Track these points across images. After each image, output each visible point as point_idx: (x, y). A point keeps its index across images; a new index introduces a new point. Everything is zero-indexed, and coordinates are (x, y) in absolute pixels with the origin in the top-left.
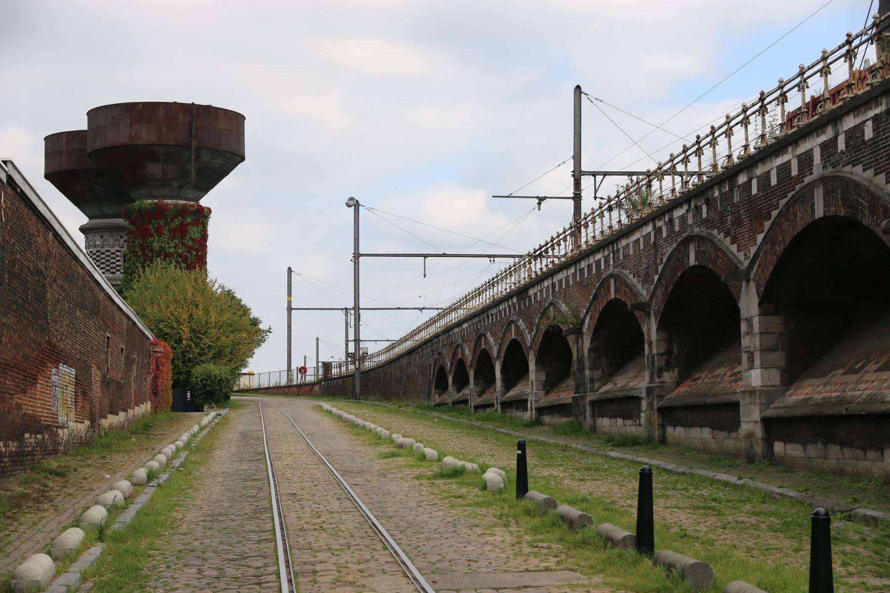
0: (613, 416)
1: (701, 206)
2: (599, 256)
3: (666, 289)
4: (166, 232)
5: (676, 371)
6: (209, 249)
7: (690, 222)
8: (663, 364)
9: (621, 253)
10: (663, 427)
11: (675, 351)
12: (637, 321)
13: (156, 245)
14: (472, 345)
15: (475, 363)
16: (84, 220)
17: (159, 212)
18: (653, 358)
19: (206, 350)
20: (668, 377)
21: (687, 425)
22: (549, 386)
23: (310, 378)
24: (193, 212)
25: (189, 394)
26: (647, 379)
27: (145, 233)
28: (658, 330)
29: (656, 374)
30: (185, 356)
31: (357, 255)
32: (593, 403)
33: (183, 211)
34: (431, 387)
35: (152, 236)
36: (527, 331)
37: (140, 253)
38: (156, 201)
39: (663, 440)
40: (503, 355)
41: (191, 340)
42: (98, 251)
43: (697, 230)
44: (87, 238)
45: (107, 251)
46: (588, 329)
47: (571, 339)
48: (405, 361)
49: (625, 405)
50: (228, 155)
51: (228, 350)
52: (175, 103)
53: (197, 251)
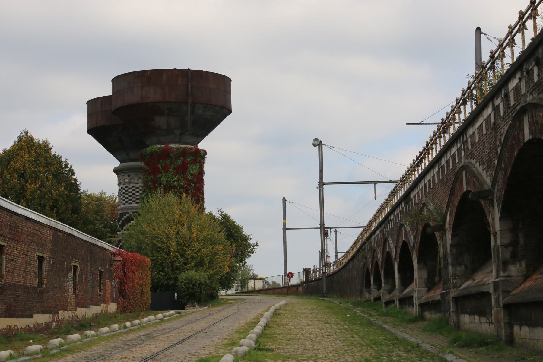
0: (471, 313)
1: (532, 69)
2: (454, 150)
3: (506, 173)
4: (171, 170)
5: (523, 263)
6: (205, 182)
7: (523, 91)
8: (508, 256)
9: (469, 143)
10: (510, 325)
11: (522, 241)
12: (484, 212)
13: (163, 180)
14: (381, 248)
15: (384, 265)
16: (117, 163)
17: (165, 154)
18: (498, 249)
19: (190, 260)
20: (514, 270)
21: (532, 324)
22: (430, 284)
23: (294, 281)
24: (192, 153)
25: (176, 295)
26: (494, 274)
27: (155, 171)
28: (501, 219)
29: (501, 267)
30: (173, 265)
31: (322, 184)
32: (456, 300)
33: (184, 153)
34: (362, 286)
35: (161, 173)
36: (411, 232)
37: (152, 187)
38: (163, 146)
39: (511, 341)
40: (398, 256)
41: (178, 252)
42: (126, 187)
43: (529, 99)
44: (119, 177)
45: (133, 187)
46: (449, 225)
47: (437, 234)
48: (350, 265)
49: (476, 302)
50: (217, 108)
51: (207, 260)
52: (175, 69)
53: (195, 183)
